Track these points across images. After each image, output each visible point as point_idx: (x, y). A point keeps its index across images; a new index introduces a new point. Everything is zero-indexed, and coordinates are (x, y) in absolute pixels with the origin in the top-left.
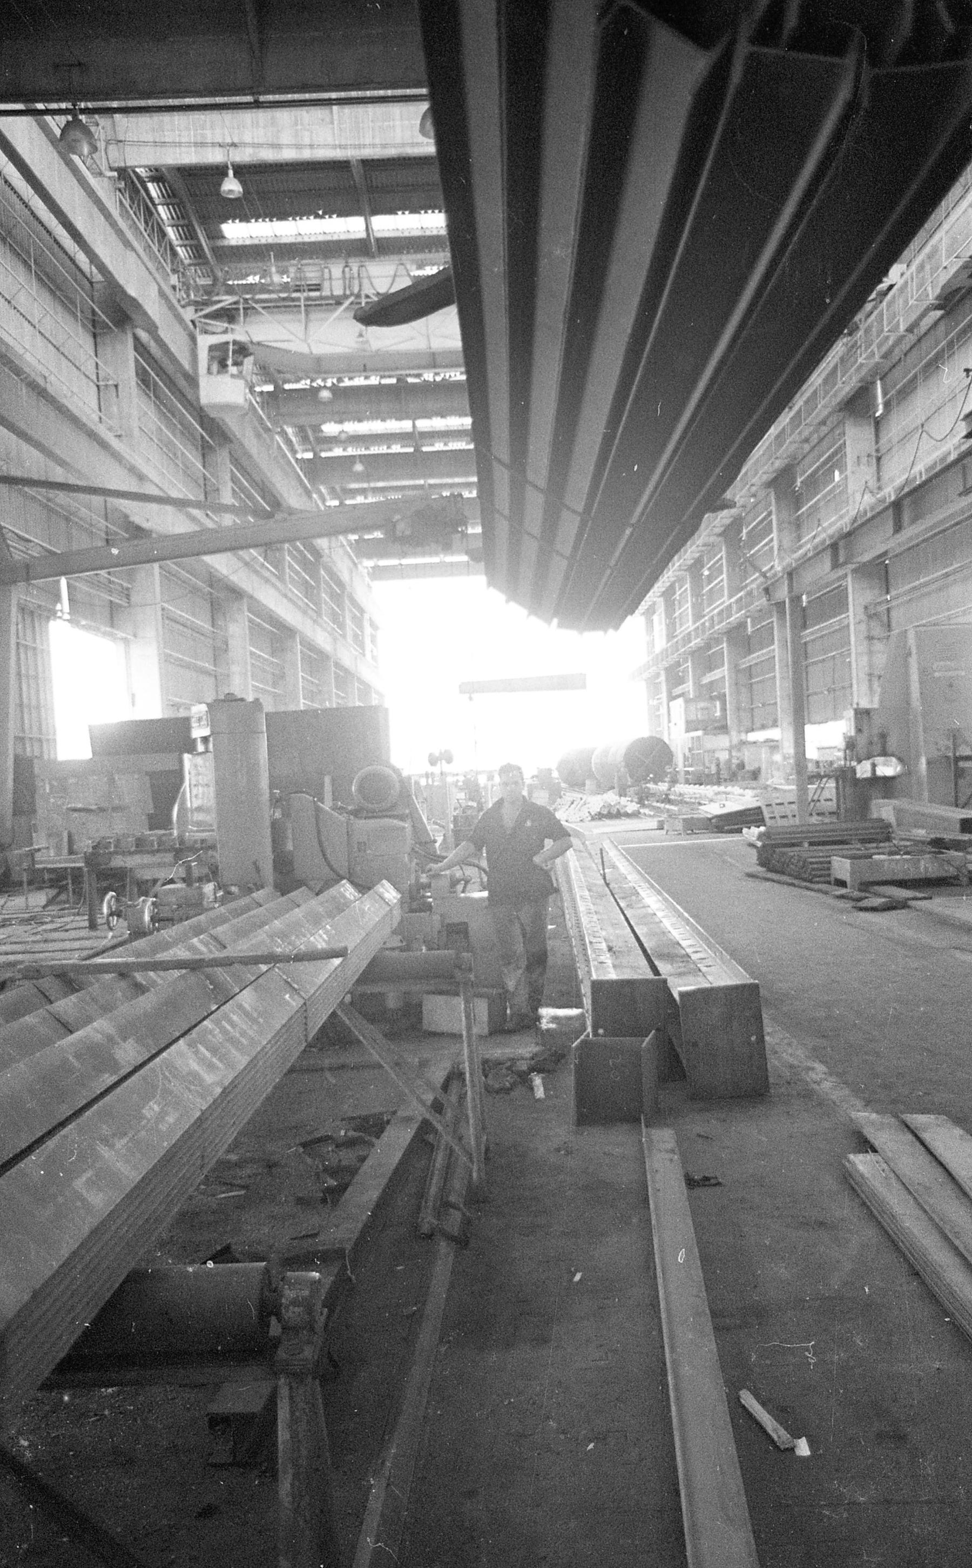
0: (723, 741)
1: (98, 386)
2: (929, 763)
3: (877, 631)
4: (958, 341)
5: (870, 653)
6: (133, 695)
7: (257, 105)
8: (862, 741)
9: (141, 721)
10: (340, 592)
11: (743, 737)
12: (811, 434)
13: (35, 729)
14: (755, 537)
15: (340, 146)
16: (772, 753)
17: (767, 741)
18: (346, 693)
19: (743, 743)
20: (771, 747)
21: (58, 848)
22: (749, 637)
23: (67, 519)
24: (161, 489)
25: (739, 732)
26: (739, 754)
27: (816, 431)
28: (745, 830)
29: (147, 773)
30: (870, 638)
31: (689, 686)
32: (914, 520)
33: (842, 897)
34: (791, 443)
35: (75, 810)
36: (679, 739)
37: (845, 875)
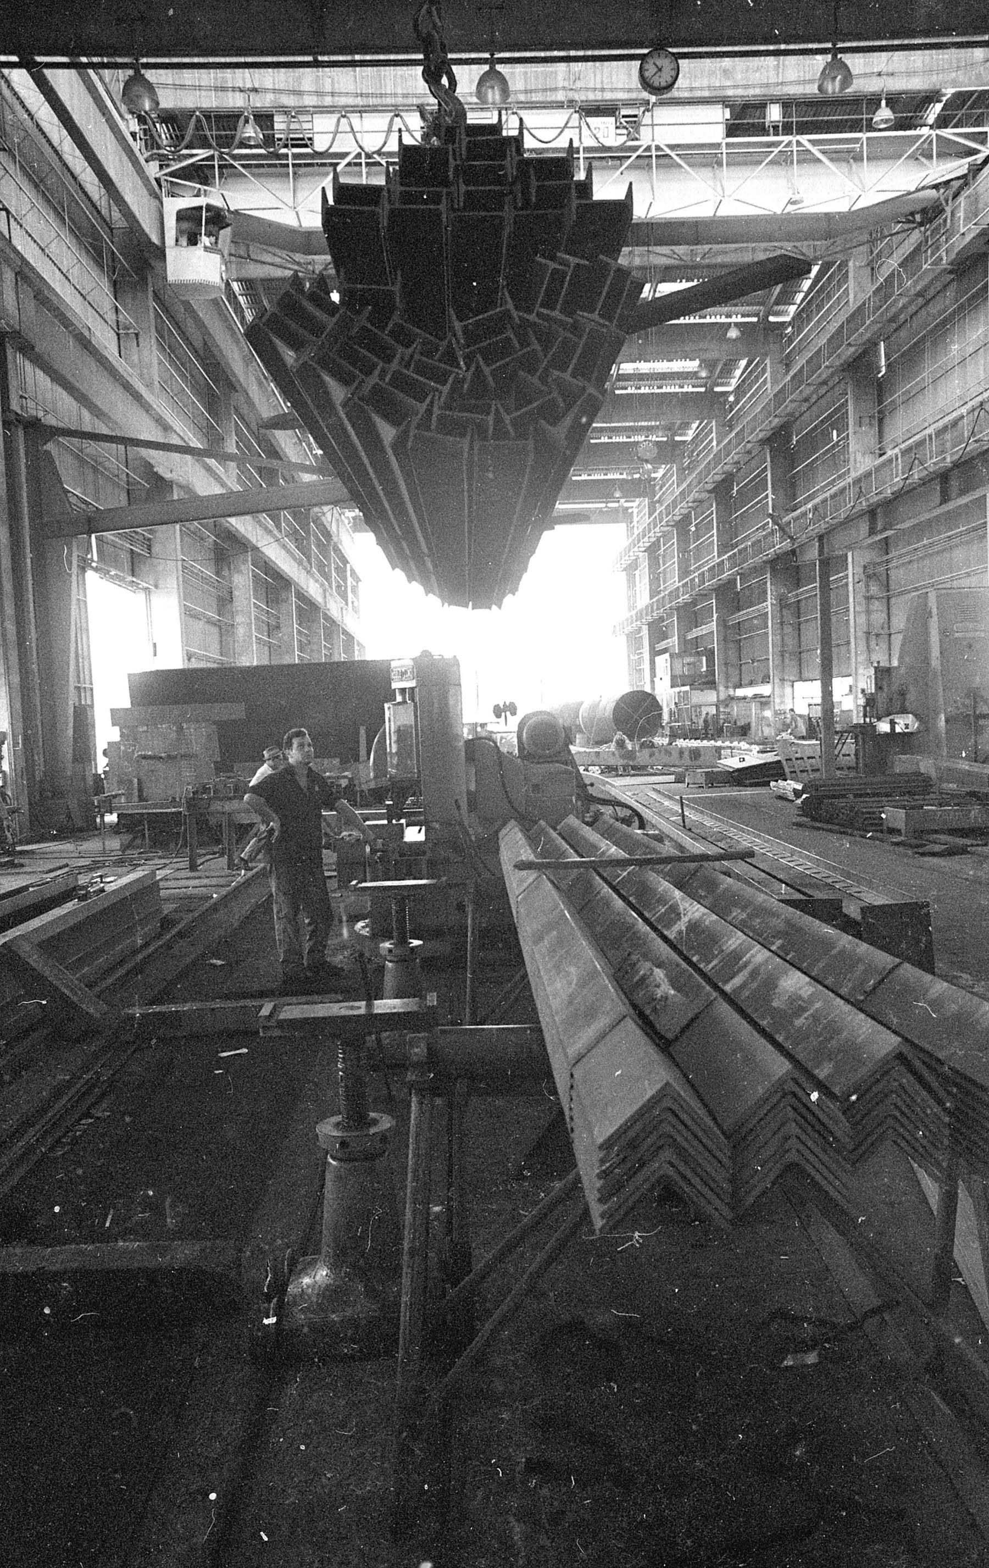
0: (711, 696)
1: (118, 335)
2: (947, 721)
3: (874, 589)
4: (970, 305)
5: (868, 612)
6: (155, 645)
7: (316, 64)
8: (882, 698)
9: (162, 671)
10: (327, 541)
11: (731, 692)
12: (812, 393)
13: (87, 682)
14: (744, 496)
15: (361, 95)
16: (762, 710)
17: (755, 696)
18: (332, 645)
19: (732, 698)
20: (761, 703)
21: (129, 796)
22: (739, 593)
23: (95, 470)
24: (182, 439)
25: (727, 687)
26: (727, 710)
27: (815, 391)
28: (772, 784)
29: (215, 723)
30: (869, 599)
31: (673, 641)
32: (963, 492)
33: (897, 844)
34: (791, 401)
35: (145, 757)
36: (665, 694)
37: (900, 825)
